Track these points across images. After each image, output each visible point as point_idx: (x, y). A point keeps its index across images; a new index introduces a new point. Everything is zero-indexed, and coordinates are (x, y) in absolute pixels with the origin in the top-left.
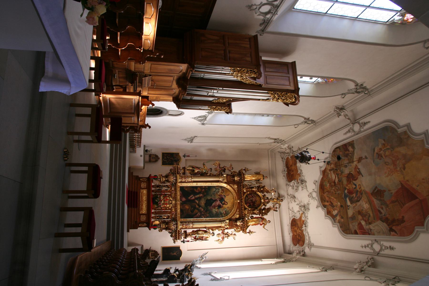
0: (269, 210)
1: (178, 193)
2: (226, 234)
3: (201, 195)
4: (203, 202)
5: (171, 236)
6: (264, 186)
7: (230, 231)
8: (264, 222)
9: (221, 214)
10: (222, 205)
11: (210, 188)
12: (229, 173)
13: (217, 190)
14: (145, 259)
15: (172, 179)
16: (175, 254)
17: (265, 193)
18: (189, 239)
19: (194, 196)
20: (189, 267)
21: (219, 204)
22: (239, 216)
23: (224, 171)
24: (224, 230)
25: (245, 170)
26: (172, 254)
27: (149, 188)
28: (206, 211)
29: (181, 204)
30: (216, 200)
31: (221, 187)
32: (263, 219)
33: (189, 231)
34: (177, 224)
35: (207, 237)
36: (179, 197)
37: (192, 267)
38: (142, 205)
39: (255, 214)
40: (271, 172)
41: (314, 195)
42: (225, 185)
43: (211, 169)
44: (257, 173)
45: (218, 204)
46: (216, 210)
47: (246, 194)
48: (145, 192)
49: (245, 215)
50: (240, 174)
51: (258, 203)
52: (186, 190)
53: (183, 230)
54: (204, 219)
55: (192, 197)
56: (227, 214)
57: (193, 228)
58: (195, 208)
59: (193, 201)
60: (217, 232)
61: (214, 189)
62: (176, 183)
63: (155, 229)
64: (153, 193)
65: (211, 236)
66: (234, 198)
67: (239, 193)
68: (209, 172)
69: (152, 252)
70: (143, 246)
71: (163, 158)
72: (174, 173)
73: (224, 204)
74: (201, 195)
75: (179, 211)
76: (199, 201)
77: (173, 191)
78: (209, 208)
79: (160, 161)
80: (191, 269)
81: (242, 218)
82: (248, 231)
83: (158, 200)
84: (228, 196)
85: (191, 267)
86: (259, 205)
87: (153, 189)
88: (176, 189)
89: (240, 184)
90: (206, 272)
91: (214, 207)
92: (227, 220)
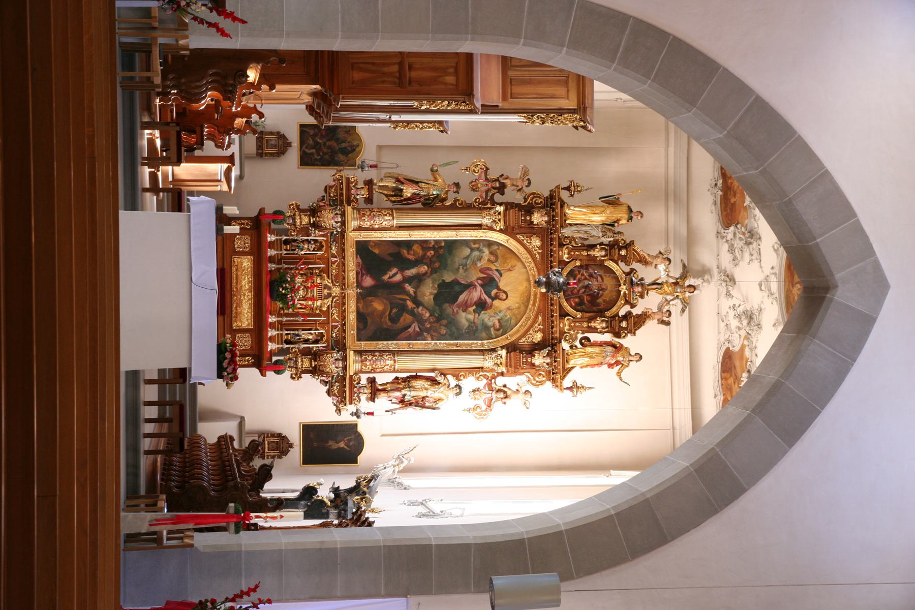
0: (641, 320)
1: (352, 263)
2: (499, 391)
3: (424, 269)
4: (428, 292)
5: (329, 393)
6: (632, 242)
7: (512, 382)
8: (620, 359)
9: (486, 328)
10: (489, 300)
11: (451, 245)
12: (518, 198)
13: (476, 253)
14: (252, 459)
15: (330, 219)
16: (342, 445)
17: (635, 265)
18: (383, 402)
19: (402, 270)
20: (364, 483)
21: (480, 298)
22: (544, 338)
23: (501, 189)
24: (494, 377)
25: (568, 189)
26: (333, 445)
27: (257, 252)
28: (438, 320)
29: (360, 298)
30: (469, 286)
31: (489, 244)
32: (617, 348)
33: (382, 379)
34: (345, 359)
35: (437, 401)
36: (351, 276)
37: (372, 484)
38: (239, 304)
39: (594, 330)
40: (671, 187)
41: (774, 286)
42: (501, 238)
43: (457, 185)
44: (611, 201)
45: (475, 299)
46: (471, 317)
47: (568, 269)
48: (246, 263)
49: (562, 333)
50: (552, 203)
51: (607, 295)
52: (376, 251)
53: (364, 378)
54: (431, 344)
55: (394, 275)
56: (503, 328)
57: (394, 371)
58: (403, 308)
59: (398, 287)
60: (469, 383)
61: (467, 251)
62: (343, 234)
63: (278, 372)
64: (272, 266)
65: (451, 394)
66: (528, 280)
67: (547, 261)
68: (451, 197)
69: (272, 439)
70: (242, 418)
71: (302, 142)
72: (338, 197)
73: (496, 297)
74: (424, 269)
75: (352, 317)
76: (416, 288)
77: (333, 256)
78: (449, 309)
79: (293, 155)
80: (368, 488)
81: (550, 344)
82: (567, 382)
83: (285, 289)
84: (512, 274)
85: (370, 481)
86: (613, 303)
87: (271, 252)
88: (343, 250)
89: (550, 236)
90: (413, 499)
91: (465, 306)
92: (502, 348)
